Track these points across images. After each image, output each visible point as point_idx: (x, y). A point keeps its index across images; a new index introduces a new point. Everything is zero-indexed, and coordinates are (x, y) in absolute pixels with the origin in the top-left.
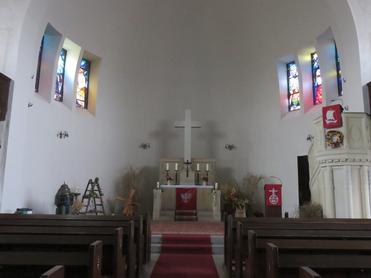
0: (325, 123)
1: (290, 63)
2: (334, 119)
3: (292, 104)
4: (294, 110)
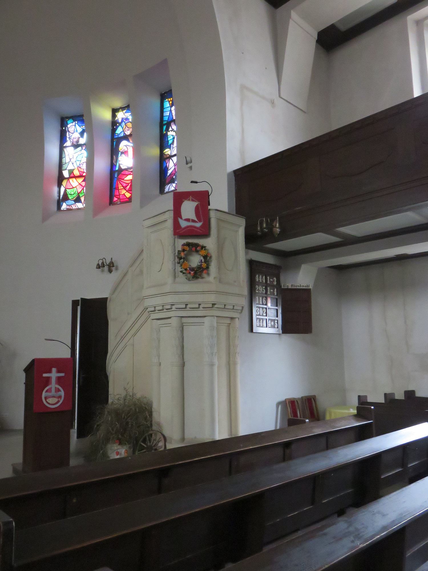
0: (176, 225)
1: (69, 118)
2: (196, 219)
3: (66, 198)
4: (68, 210)
